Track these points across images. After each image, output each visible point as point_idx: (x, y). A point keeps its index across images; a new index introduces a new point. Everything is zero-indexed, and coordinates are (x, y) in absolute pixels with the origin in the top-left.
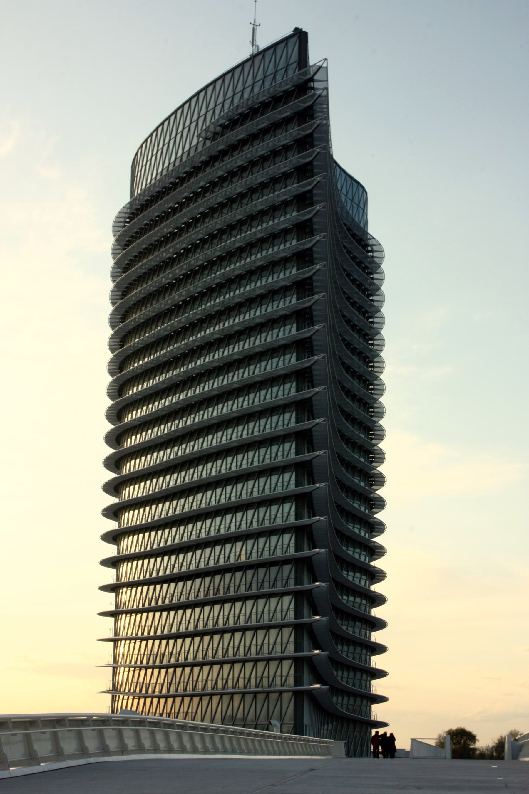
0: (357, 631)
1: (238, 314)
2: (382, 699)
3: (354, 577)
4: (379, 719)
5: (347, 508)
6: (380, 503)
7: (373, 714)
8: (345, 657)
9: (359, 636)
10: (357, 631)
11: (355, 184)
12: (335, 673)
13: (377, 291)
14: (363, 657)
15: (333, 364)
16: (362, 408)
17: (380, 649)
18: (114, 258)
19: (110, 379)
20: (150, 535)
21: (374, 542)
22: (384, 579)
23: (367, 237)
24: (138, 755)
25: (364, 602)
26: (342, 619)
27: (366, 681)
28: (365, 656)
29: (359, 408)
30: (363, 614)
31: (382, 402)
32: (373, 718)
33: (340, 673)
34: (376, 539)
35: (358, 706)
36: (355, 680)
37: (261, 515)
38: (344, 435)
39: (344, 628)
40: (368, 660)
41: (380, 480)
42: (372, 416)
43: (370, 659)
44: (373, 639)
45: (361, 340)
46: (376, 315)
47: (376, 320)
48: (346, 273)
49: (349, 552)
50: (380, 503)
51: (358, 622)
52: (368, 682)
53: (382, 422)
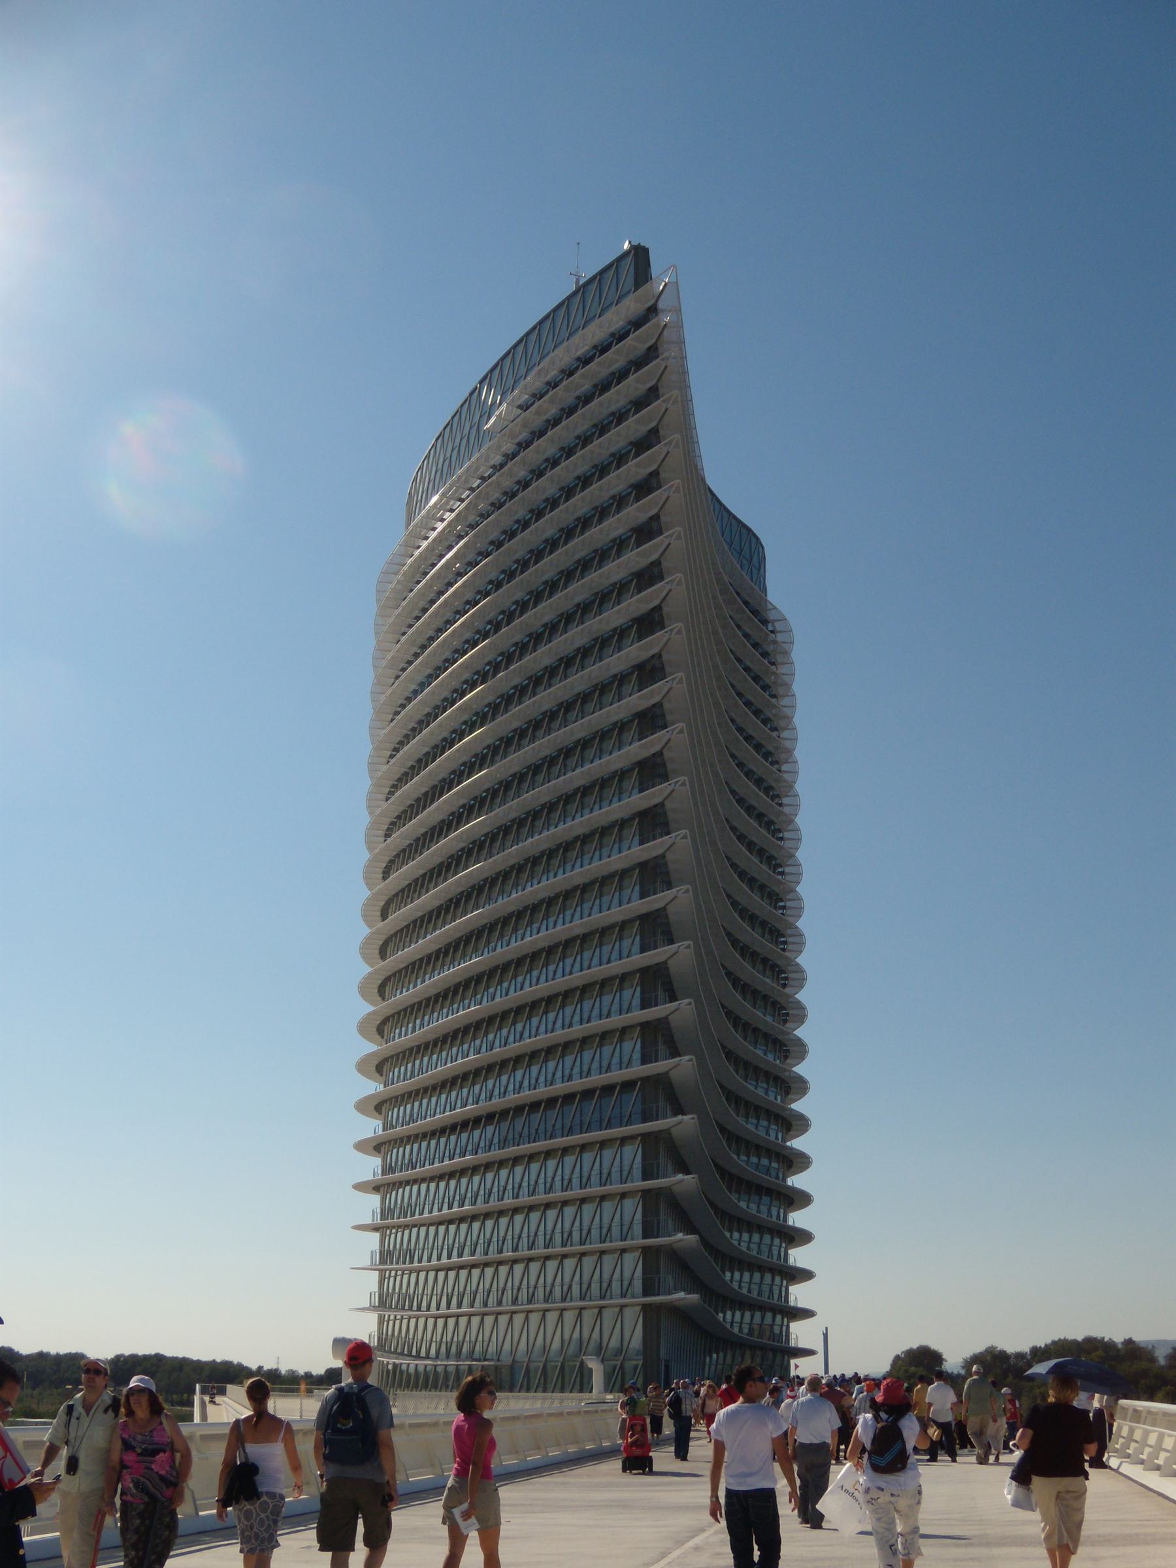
0: (764, 1208)
1: (562, 818)
3: (740, 1241)
4: (801, 1345)
6: (797, 1124)
7: (792, 1299)
9: (768, 1257)
11: (744, 531)
12: (728, 1234)
13: (789, 824)
15: (714, 682)
16: (768, 972)
17: (801, 1237)
18: (371, 813)
19: (366, 931)
20: (429, 1144)
21: (791, 1149)
23: (766, 606)
25: (775, 1165)
26: (738, 1192)
28: (778, 1248)
29: (763, 936)
31: (787, 616)
32: (792, 1344)
34: (793, 1069)
35: (769, 1325)
36: (763, 1286)
37: (606, 1165)
38: (738, 941)
39: (743, 1205)
41: (799, 1087)
42: (784, 950)
43: (786, 1254)
44: (790, 1223)
45: (764, 867)
46: (788, 897)
47: (787, 870)
48: (736, 761)
49: (749, 1126)
50: (798, 1162)
51: (765, 1196)
52: (783, 1289)
53: (800, 924)
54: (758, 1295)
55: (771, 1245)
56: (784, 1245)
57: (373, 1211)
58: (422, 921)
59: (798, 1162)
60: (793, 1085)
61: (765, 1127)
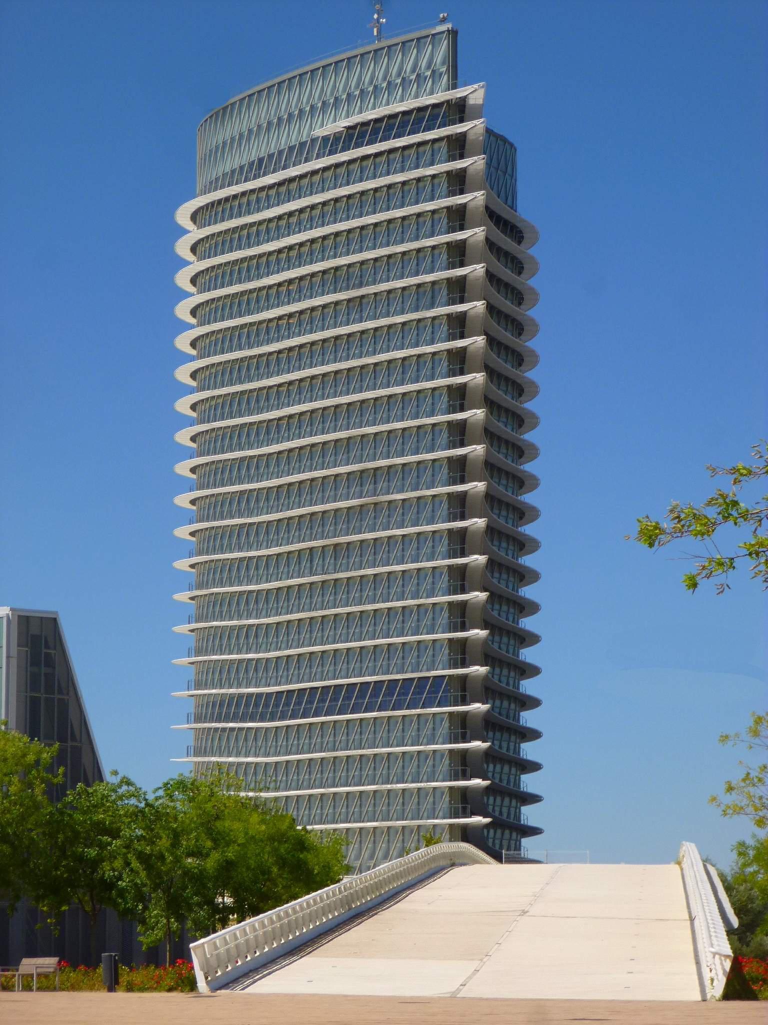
0: (505, 745)
2: (534, 831)
5: (504, 247)
8: (497, 682)
10: (505, 745)
14: (512, 745)
17: (532, 735)
21: (524, 441)
22: (537, 550)
24: (421, 995)
25: (512, 610)
27: (516, 775)
30: (511, 625)
33: (491, 767)
34: (528, 374)
40: (517, 715)
43: (519, 684)
44: (522, 690)
54: (507, 784)
55: (509, 807)
56: (518, 741)
57: (189, 649)
58: (207, 209)
59: (528, 639)
60: (526, 452)
61: (504, 485)
